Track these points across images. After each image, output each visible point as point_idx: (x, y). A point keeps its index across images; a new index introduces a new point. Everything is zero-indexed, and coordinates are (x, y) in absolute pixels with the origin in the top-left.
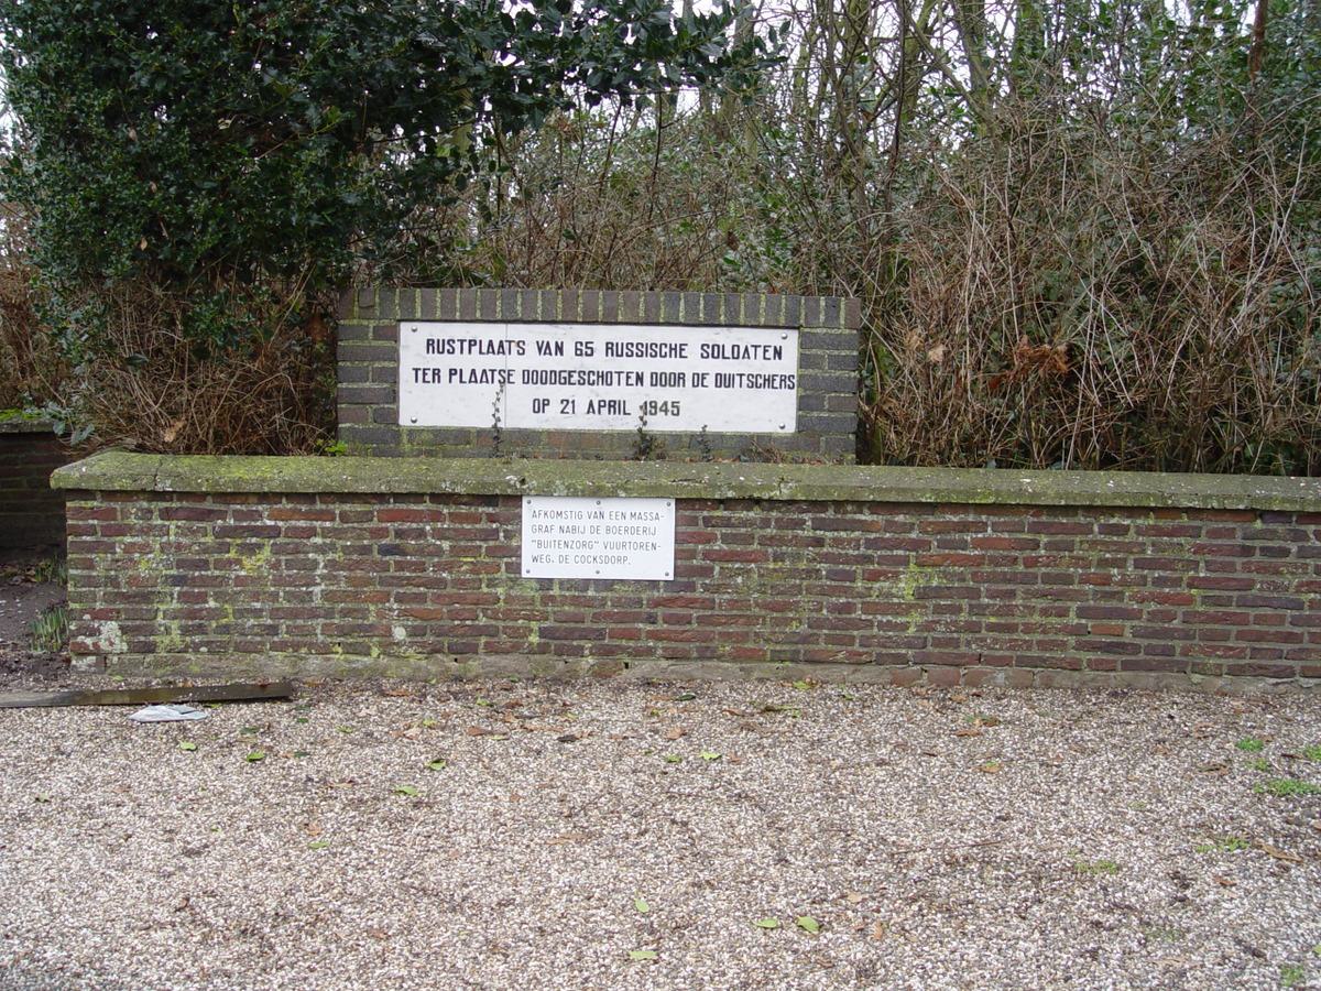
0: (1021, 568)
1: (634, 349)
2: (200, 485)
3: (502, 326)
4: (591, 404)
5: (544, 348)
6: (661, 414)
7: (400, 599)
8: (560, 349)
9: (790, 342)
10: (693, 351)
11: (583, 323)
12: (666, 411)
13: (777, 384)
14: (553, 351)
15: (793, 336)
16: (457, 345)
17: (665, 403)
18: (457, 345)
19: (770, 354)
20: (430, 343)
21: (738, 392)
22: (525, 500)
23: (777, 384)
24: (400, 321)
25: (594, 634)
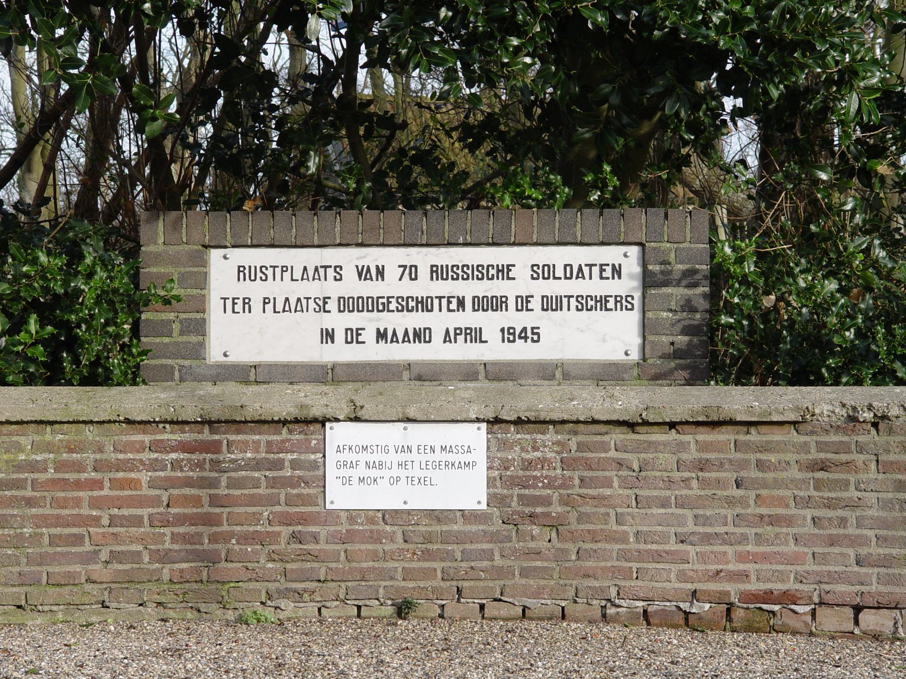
1: (459, 272)
2: (500, 428)
4: (447, 331)
5: (363, 273)
8: (380, 272)
9: (628, 258)
10: (522, 272)
11: (253, 246)
12: (526, 338)
13: (611, 305)
14: (374, 277)
15: (634, 251)
16: (270, 273)
17: (525, 329)
18: (270, 273)
19: (608, 272)
20: (240, 269)
21: (570, 317)
23: (611, 305)
24: (206, 247)
25: (413, 574)
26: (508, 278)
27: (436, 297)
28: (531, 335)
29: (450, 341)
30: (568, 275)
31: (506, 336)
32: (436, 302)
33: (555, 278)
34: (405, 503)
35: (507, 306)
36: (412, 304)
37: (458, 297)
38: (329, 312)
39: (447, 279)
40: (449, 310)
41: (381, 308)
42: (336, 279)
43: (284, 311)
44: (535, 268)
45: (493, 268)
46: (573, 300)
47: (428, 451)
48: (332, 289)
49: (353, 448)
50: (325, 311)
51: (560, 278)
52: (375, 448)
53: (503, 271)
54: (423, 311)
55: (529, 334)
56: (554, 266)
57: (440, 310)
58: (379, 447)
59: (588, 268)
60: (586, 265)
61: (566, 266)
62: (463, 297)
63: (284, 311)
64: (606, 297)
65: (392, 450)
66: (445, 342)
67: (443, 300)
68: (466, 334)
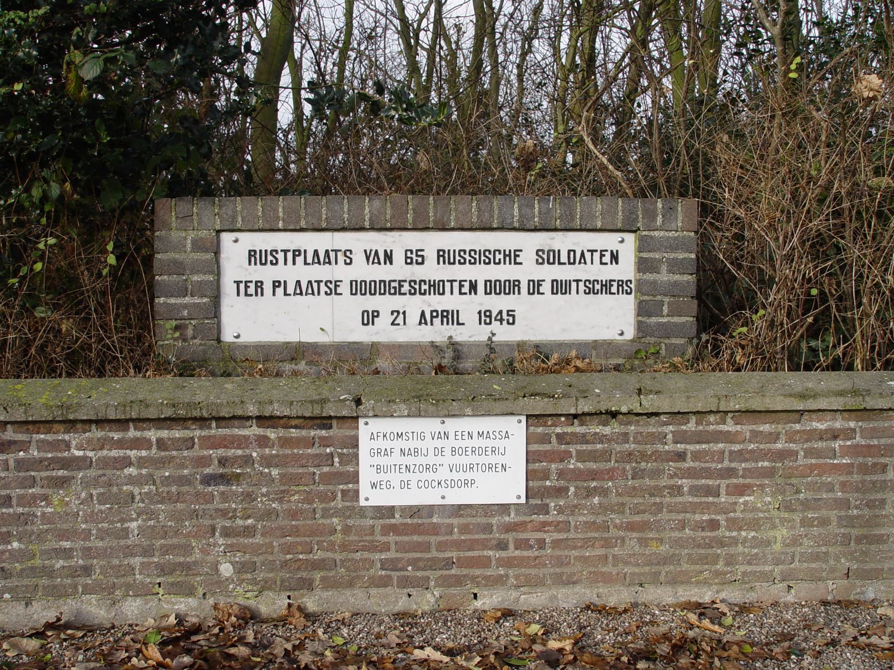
3: (328, 235)
4: (423, 314)
5: (371, 257)
8: (389, 257)
9: (627, 246)
10: (528, 257)
12: (501, 320)
14: (382, 261)
16: (280, 256)
17: (501, 312)
18: (280, 256)
19: (607, 258)
20: (252, 254)
23: (614, 289)
26: (516, 263)
27: (448, 281)
28: (510, 318)
29: (426, 323)
30: (572, 261)
31: (483, 318)
32: (448, 285)
33: (560, 263)
34: (443, 497)
35: (519, 290)
36: (598, 287)
37: (471, 281)
38: (543, 294)
39: (454, 263)
40: (246, 294)
41: (392, 291)
42: (346, 264)
43: (295, 294)
44: (540, 253)
45: (500, 253)
46: (581, 284)
47: (466, 437)
48: (339, 272)
49: (388, 436)
50: (336, 294)
51: (564, 264)
52: (410, 435)
53: (510, 256)
54: (435, 294)
55: (505, 316)
56: (559, 251)
57: (452, 293)
58: (415, 434)
59: (590, 253)
60: (588, 251)
61: (569, 251)
62: (476, 281)
63: (295, 294)
64: (611, 281)
65: (428, 437)
66: (420, 323)
67: (454, 283)
68: (443, 316)
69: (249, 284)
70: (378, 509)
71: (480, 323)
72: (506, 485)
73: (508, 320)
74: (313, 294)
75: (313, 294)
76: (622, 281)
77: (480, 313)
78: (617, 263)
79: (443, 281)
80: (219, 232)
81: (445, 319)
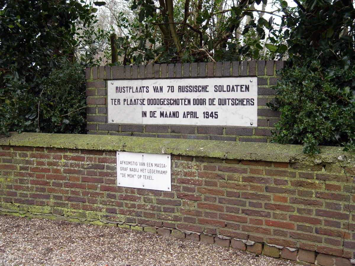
0: (217, 203)
1: (188, 89)
3: (140, 81)
5: (156, 89)
6: (210, 118)
7: (55, 197)
9: (253, 83)
12: (212, 116)
15: (255, 80)
18: (126, 89)
20: (117, 88)
22: (117, 153)
23: (245, 103)
28: (214, 115)
30: (228, 90)
31: (205, 115)
32: (180, 101)
33: (223, 91)
35: (205, 103)
37: (188, 99)
38: (215, 105)
39: (184, 92)
43: (130, 104)
44: (216, 87)
46: (230, 101)
51: (225, 91)
55: (214, 115)
56: (223, 86)
59: (236, 87)
61: (227, 86)
62: (190, 99)
63: (130, 104)
64: (243, 99)
66: (183, 117)
67: (230, 100)
68: (191, 114)
69: (186, 100)
70: (127, 189)
71: (204, 118)
72: (163, 183)
73: (215, 116)
74: (136, 104)
75: (136, 104)
76: (249, 99)
77: (204, 113)
78: (248, 91)
79: (179, 99)
80: (106, 80)
81: (192, 115)
